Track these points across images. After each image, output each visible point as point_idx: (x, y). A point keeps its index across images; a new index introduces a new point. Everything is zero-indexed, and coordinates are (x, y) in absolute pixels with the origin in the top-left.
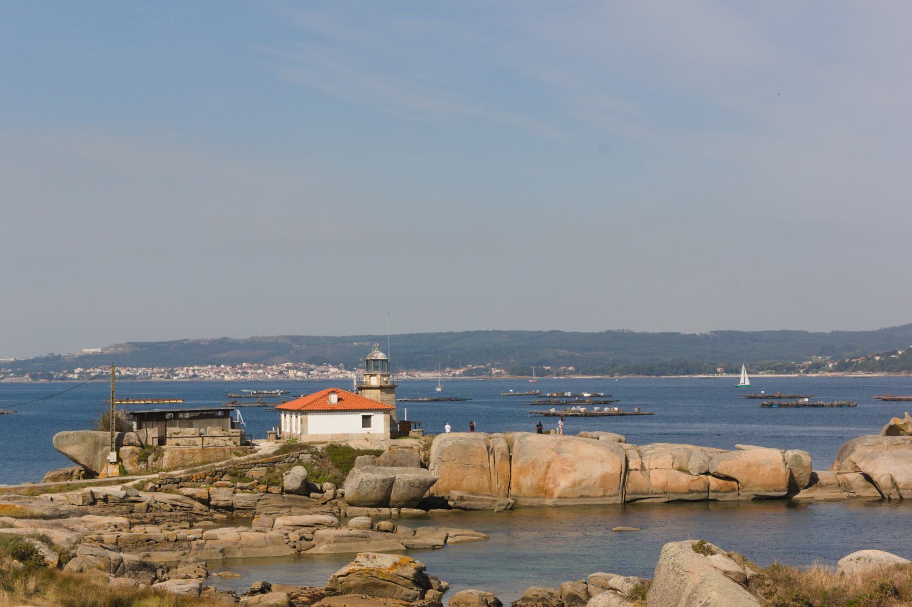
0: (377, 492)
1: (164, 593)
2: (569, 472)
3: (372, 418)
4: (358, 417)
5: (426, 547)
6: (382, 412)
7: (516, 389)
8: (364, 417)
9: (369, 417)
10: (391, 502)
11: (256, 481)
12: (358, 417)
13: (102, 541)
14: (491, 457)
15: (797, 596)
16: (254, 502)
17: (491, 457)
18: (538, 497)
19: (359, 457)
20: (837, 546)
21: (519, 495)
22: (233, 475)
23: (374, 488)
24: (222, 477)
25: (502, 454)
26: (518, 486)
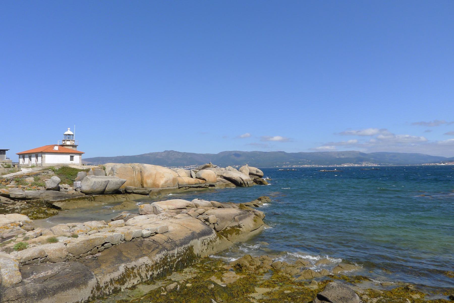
0: (101, 187)
1: (148, 208)
2: (163, 177)
3: (74, 157)
4: (68, 157)
5: (170, 197)
6: (79, 155)
7: (289, 169)
8: (71, 156)
9: (73, 156)
10: (105, 192)
11: (30, 184)
12: (68, 157)
13: (87, 198)
14: (135, 172)
15: (239, 262)
16: (39, 194)
17: (135, 172)
18: (153, 188)
19: (79, 172)
20: (197, 285)
21: (147, 187)
22: (17, 181)
23: (101, 186)
24: (10, 182)
25: (138, 171)
26: (146, 183)
